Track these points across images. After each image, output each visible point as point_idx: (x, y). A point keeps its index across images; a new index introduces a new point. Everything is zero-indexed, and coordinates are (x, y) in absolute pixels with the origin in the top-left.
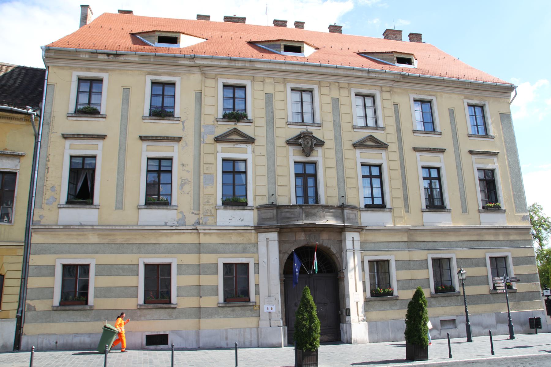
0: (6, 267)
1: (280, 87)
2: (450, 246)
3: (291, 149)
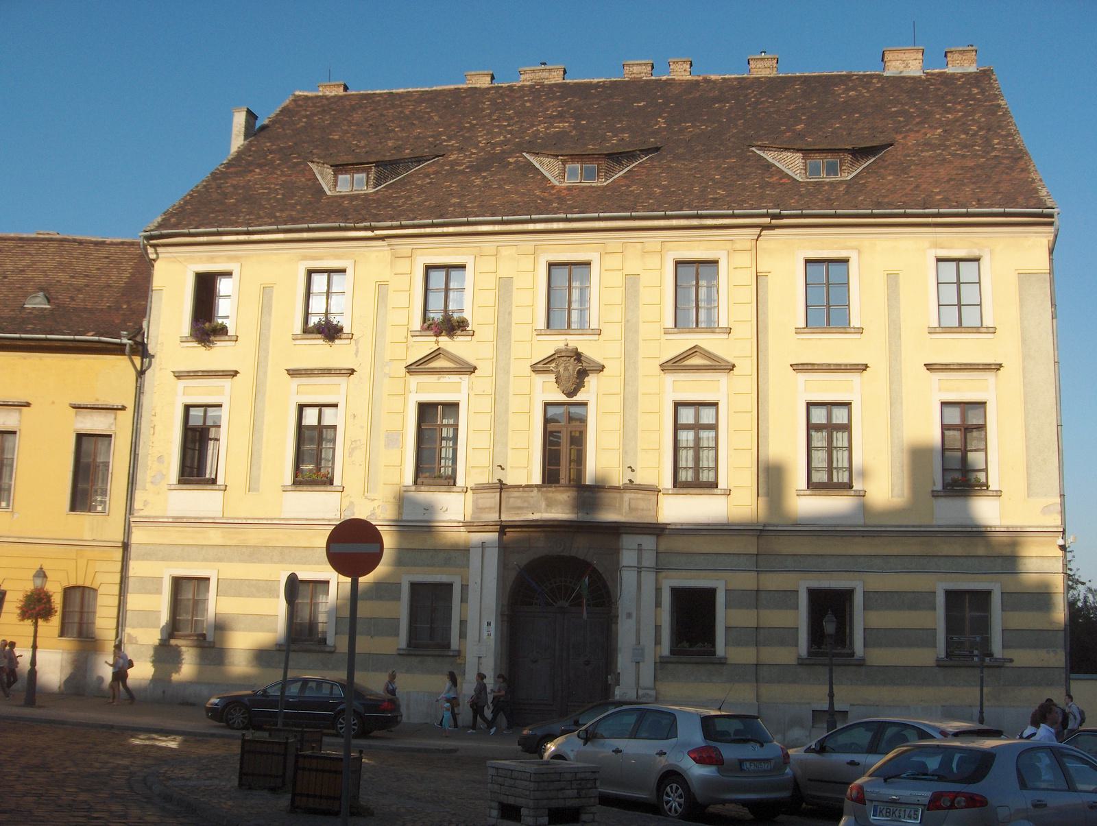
0: (100, 578)
1: (527, 263)
2: (854, 564)
3: (539, 379)
